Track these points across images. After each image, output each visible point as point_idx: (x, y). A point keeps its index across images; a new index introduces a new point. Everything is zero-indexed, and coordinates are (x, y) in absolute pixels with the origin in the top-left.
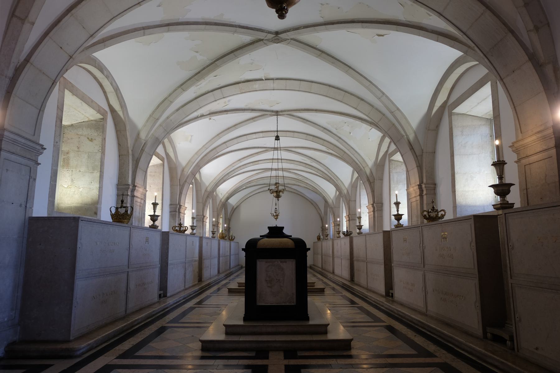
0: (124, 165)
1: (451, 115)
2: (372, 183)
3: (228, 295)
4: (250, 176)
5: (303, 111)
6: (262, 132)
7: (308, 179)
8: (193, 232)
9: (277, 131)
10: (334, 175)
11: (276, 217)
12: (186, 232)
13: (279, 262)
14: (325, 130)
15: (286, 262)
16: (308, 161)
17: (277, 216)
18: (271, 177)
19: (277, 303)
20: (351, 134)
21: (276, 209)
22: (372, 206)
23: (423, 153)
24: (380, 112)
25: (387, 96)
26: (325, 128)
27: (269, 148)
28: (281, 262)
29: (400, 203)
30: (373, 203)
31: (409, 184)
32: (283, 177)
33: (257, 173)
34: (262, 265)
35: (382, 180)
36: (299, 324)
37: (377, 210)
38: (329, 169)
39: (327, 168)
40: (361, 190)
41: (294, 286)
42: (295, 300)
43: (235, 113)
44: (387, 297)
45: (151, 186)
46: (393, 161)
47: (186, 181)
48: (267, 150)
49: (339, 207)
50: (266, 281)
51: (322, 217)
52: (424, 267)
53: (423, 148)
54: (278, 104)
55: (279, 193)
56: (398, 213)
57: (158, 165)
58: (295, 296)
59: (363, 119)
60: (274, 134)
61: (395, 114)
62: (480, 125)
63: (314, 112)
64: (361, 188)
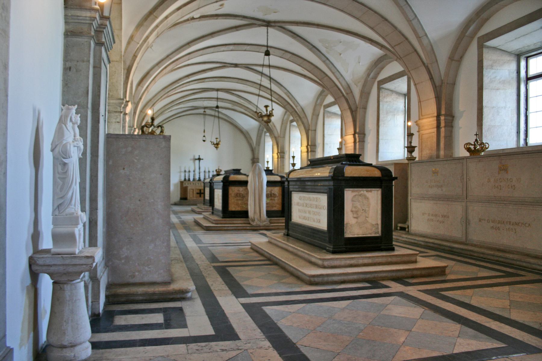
0: (115, 73)
1: (481, 47)
5: (302, 25)
6: (234, 44)
11: (216, 146)
13: (365, 192)
15: (371, 191)
17: (217, 144)
19: (358, 235)
20: (342, 55)
21: (204, 136)
23: (443, 84)
24: (403, 35)
25: (418, 20)
26: (314, 47)
27: (229, 64)
31: (421, 115)
34: (349, 194)
36: (391, 254)
37: (359, 142)
39: (288, 91)
40: (325, 119)
41: (379, 217)
43: (226, 19)
49: (284, 137)
50: (352, 211)
52: (466, 199)
53: (443, 78)
54: (275, 12)
56: (411, 145)
62: (509, 60)
63: (314, 26)
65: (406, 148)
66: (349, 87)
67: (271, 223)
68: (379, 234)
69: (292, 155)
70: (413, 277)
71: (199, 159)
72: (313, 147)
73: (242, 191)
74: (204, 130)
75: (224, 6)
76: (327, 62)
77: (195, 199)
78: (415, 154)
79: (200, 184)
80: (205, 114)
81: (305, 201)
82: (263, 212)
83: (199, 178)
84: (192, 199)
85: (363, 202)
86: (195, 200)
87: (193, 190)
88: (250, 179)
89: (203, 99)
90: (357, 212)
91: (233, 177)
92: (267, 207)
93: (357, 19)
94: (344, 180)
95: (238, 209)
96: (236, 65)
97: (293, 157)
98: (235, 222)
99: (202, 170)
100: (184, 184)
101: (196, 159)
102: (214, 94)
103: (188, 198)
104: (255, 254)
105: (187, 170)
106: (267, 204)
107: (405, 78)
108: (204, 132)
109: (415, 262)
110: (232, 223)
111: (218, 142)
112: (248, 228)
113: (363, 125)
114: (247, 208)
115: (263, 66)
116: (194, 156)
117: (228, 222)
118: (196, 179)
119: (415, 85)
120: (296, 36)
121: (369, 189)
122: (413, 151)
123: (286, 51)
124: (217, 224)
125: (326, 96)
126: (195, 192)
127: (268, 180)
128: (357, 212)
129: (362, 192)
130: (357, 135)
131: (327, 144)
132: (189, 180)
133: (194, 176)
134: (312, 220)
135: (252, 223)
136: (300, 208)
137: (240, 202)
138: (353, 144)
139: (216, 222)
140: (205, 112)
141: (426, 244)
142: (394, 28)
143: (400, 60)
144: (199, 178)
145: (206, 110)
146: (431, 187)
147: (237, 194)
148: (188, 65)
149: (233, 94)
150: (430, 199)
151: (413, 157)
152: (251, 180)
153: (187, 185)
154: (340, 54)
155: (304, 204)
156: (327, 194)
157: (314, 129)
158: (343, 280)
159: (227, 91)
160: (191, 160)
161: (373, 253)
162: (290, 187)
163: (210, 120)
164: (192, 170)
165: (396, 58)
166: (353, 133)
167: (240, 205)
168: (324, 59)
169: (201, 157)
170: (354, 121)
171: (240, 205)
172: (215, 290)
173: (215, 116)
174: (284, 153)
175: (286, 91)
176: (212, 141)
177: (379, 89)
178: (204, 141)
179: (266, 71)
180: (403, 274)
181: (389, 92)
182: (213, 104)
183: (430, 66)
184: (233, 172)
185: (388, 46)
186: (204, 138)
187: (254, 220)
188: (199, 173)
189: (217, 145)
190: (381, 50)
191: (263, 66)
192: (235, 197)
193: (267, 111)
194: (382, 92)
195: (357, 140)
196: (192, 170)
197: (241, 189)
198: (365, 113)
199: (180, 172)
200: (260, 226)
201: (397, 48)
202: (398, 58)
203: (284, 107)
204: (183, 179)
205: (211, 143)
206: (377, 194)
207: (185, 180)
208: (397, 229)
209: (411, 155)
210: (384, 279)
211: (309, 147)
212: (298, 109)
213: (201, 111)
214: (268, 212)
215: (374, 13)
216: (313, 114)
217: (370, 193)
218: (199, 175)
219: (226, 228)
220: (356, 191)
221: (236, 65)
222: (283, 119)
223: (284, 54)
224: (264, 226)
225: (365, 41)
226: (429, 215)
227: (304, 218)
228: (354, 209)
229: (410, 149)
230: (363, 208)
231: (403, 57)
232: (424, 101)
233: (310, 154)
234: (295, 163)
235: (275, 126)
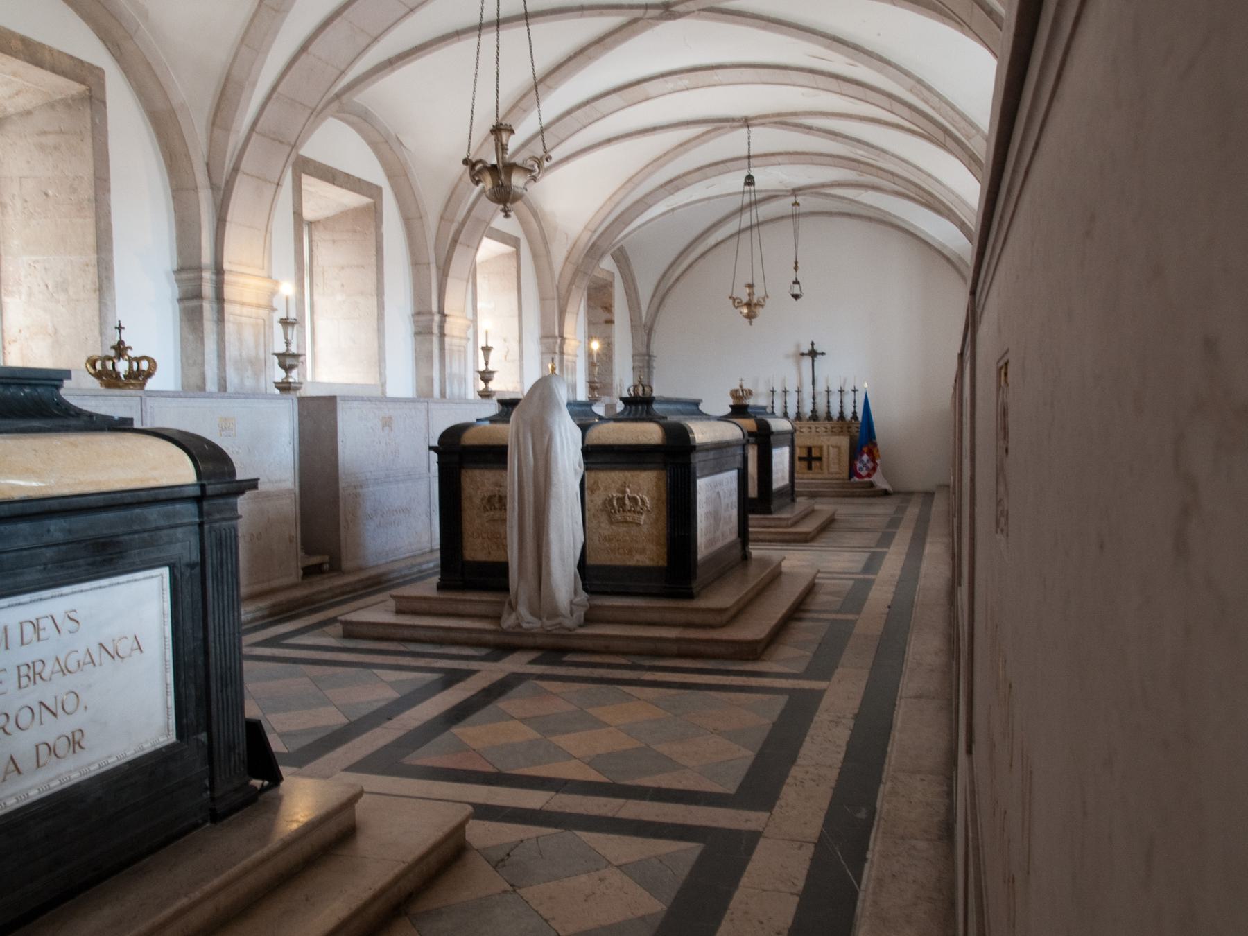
4: (660, 158)
7: (887, 157)
8: (287, 377)
10: (951, 113)
12: (151, 385)
16: (838, 63)
18: (749, 157)
21: (796, 282)
38: (929, 88)
39: (919, 81)
45: (46, 194)
47: (236, 169)
48: (635, 21)
55: (509, 175)
57: (70, 101)
69: (482, 343)
71: (813, 354)
74: (796, 263)
79: (813, 430)
97: (487, 350)
99: (821, 387)
101: (803, 354)
105: (779, 389)
108: (796, 268)
116: (798, 346)
118: (805, 414)
133: (798, 407)
140: (796, 204)
145: (799, 199)
147: (490, 499)
149: (809, 129)
160: (787, 356)
164: (792, 389)
169: (818, 348)
172: (812, 738)
175: (911, 82)
176: (734, 296)
178: (796, 297)
186: (797, 286)
192: (486, 510)
196: (792, 389)
205: (731, 301)
212: (972, 145)
218: (814, 403)
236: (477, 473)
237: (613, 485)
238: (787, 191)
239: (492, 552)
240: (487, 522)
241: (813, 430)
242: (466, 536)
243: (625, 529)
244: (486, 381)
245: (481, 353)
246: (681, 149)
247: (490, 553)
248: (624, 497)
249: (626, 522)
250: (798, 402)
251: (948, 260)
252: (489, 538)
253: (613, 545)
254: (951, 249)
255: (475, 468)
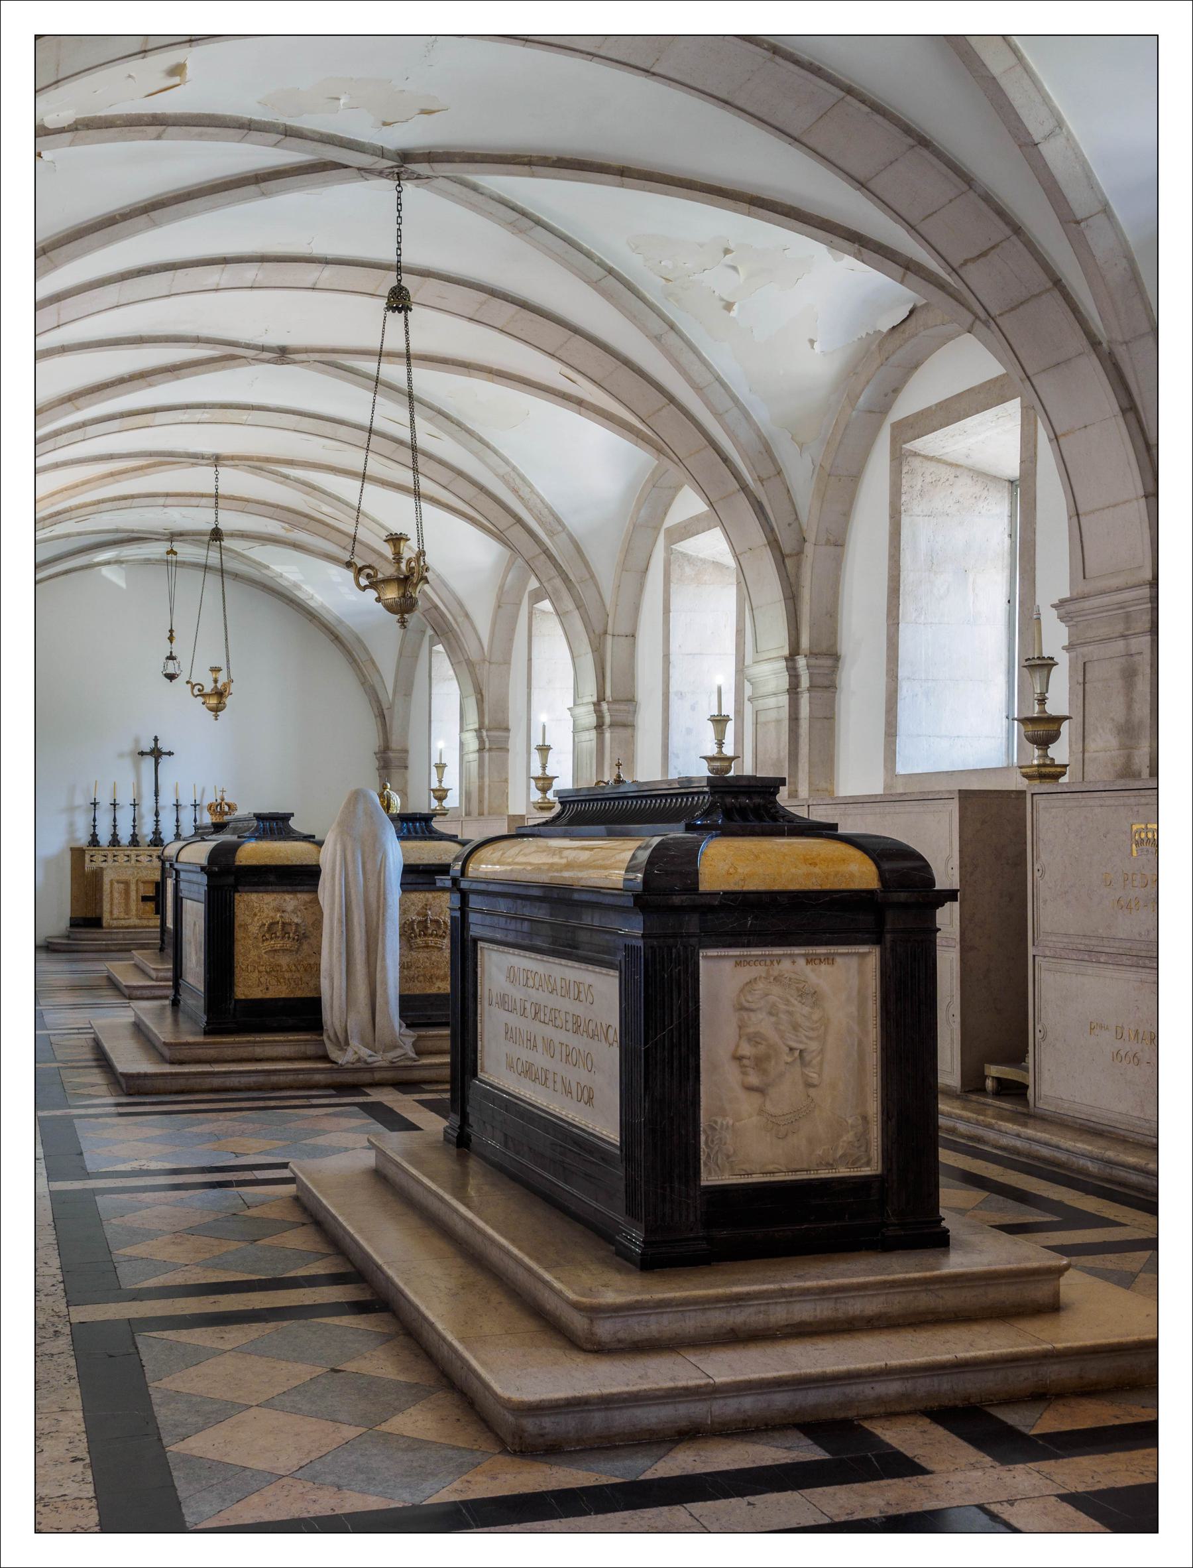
2: (790, 556)
3: (113, 1110)
4: (77, 486)
6: (263, 259)
9: (399, 269)
13: (801, 962)
14: (610, 277)
15: (830, 959)
17: (220, 694)
21: (171, 658)
22: (788, 669)
27: (248, 346)
28: (808, 962)
29: (1056, 664)
30: (791, 655)
32: (217, 496)
33: (112, 474)
35: (842, 546)
37: (812, 687)
40: (674, 587)
42: (876, 1152)
43: (200, 137)
44: (974, 1097)
46: (920, 459)
48: (233, 357)
49: (507, 662)
50: (738, 1058)
51: (385, 706)
58: (875, 1132)
59: (871, 240)
60: (316, 274)
61: (1086, 232)
64: (674, 578)
65: (1016, 722)
66: (767, 450)
67: (420, 1053)
68: (872, 1168)
69: (537, 740)
70: (1041, 1396)
71: (157, 753)
72: (622, 707)
73: (294, 912)
74: (171, 631)
75: (189, 72)
76: (671, 338)
77: (134, 921)
78: (1060, 752)
79: (133, 858)
80: (171, 562)
81: (532, 992)
82: (387, 1003)
83: (157, 832)
84: (123, 922)
85: (790, 1013)
86: (135, 927)
87: (127, 883)
88: (327, 858)
89: (161, 501)
90: (760, 1063)
91: (254, 852)
92: (404, 979)
93: (795, 140)
94: (694, 908)
95: (280, 991)
96: (283, 354)
97: (544, 749)
98: (259, 1051)
99: (167, 799)
100: (87, 858)
101: (142, 754)
102: (200, 479)
103: (106, 919)
104: (299, 1240)
105: (105, 801)
106: (404, 966)
107: (1014, 407)
108: (171, 639)
109: (1053, 1308)
110: (245, 1055)
111: (219, 685)
112: (319, 1078)
113: (830, 617)
114: (318, 988)
115: (381, 354)
116: (137, 741)
117: (229, 1052)
119: (1055, 438)
120: (532, 224)
121: (822, 950)
122: (1054, 737)
123: (494, 293)
124: (181, 1063)
125: (677, 488)
126: (133, 895)
127: (411, 861)
128: (760, 1063)
129: (786, 964)
130: (802, 662)
131: (681, 695)
132: (115, 841)
134: (559, 1086)
135: (334, 1053)
136: (513, 1020)
137: (284, 960)
138: (784, 700)
139: (173, 1054)
140: (172, 552)
141: (1108, 1170)
142: (958, 181)
143: (989, 327)
144: (157, 832)
145: (177, 546)
146: (1128, 907)
148: (64, 349)
150: (1125, 960)
151: (1053, 765)
152: (334, 862)
153: (99, 862)
154: (729, 306)
155: (528, 1005)
156: (617, 973)
157: (628, 632)
158: (683, 1424)
159: (258, 464)
161: (842, 1266)
162: (473, 918)
163: (189, 583)
164: (125, 799)
165: (969, 318)
166: (786, 652)
167: (287, 975)
168: (657, 326)
169: (164, 746)
170: (792, 598)
171: (287, 975)
173: (206, 568)
174: (507, 729)
177: (898, 458)
178: (171, 677)
179: (394, 372)
180: (988, 1382)
181: (945, 472)
182: (201, 519)
183: (1121, 352)
184: (257, 829)
185: (932, 264)
187: (347, 1043)
188: (157, 815)
189: (217, 699)
190: (902, 282)
191: (381, 354)
193: (398, 557)
194: (912, 472)
195: (805, 682)
196: (125, 799)
197: (290, 903)
198: (838, 563)
199: (71, 809)
200: (371, 1070)
201: (973, 274)
202: (977, 317)
203: (499, 536)
204: (83, 839)
206: (861, 972)
207: (94, 841)
208: (981, 1090)
209: (1046, 756)
210: (892, 1412)
211: (605, 706)
213: (158, 550)
214: (407, 1002)
215: (868, 109)
216: (624, 567)
217: (824, 967)
219: (217, 1082)
220: (759, 960)
221: (283, 354)
222: (501, 587)
223: (482, 304)
224: (393, 1067)
225: (830, 245)
226: (1119, 1034)
227: (528, 1072)
228: (746, 1049)
229: (1041, 729)
230: (794, 1045)
231: (1001, 315)
232: (1093, 512)
233: (608, 735)
234: (549, 773)
235: (467, 615)
236: (254, 896)
237: (413, 907)
238: (164, 534)
239: (270, 987)
240: (265, 953)
241: (133, 858)
242: (237, 971)
243: (425, 955)
244: (440, 799)
245: (434, 770)
246: (111, 479)
247: (267, 989)
248: (426, 920)
249: (427, 947)
250: (134, 821)
251: (336, 638)
252: (266, 972)
253: (412, 973)
254: (348, 626)
255: (251, 892)
